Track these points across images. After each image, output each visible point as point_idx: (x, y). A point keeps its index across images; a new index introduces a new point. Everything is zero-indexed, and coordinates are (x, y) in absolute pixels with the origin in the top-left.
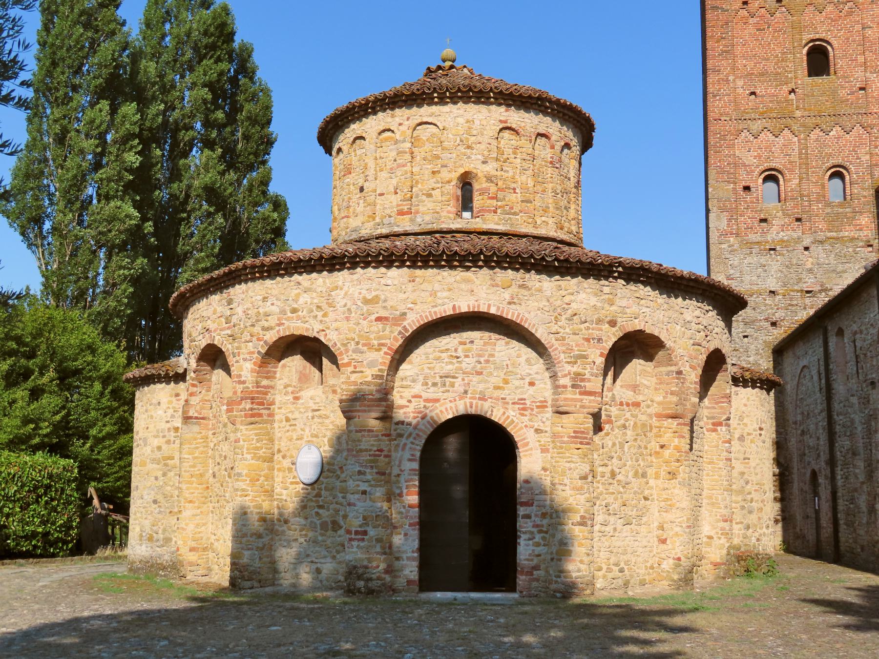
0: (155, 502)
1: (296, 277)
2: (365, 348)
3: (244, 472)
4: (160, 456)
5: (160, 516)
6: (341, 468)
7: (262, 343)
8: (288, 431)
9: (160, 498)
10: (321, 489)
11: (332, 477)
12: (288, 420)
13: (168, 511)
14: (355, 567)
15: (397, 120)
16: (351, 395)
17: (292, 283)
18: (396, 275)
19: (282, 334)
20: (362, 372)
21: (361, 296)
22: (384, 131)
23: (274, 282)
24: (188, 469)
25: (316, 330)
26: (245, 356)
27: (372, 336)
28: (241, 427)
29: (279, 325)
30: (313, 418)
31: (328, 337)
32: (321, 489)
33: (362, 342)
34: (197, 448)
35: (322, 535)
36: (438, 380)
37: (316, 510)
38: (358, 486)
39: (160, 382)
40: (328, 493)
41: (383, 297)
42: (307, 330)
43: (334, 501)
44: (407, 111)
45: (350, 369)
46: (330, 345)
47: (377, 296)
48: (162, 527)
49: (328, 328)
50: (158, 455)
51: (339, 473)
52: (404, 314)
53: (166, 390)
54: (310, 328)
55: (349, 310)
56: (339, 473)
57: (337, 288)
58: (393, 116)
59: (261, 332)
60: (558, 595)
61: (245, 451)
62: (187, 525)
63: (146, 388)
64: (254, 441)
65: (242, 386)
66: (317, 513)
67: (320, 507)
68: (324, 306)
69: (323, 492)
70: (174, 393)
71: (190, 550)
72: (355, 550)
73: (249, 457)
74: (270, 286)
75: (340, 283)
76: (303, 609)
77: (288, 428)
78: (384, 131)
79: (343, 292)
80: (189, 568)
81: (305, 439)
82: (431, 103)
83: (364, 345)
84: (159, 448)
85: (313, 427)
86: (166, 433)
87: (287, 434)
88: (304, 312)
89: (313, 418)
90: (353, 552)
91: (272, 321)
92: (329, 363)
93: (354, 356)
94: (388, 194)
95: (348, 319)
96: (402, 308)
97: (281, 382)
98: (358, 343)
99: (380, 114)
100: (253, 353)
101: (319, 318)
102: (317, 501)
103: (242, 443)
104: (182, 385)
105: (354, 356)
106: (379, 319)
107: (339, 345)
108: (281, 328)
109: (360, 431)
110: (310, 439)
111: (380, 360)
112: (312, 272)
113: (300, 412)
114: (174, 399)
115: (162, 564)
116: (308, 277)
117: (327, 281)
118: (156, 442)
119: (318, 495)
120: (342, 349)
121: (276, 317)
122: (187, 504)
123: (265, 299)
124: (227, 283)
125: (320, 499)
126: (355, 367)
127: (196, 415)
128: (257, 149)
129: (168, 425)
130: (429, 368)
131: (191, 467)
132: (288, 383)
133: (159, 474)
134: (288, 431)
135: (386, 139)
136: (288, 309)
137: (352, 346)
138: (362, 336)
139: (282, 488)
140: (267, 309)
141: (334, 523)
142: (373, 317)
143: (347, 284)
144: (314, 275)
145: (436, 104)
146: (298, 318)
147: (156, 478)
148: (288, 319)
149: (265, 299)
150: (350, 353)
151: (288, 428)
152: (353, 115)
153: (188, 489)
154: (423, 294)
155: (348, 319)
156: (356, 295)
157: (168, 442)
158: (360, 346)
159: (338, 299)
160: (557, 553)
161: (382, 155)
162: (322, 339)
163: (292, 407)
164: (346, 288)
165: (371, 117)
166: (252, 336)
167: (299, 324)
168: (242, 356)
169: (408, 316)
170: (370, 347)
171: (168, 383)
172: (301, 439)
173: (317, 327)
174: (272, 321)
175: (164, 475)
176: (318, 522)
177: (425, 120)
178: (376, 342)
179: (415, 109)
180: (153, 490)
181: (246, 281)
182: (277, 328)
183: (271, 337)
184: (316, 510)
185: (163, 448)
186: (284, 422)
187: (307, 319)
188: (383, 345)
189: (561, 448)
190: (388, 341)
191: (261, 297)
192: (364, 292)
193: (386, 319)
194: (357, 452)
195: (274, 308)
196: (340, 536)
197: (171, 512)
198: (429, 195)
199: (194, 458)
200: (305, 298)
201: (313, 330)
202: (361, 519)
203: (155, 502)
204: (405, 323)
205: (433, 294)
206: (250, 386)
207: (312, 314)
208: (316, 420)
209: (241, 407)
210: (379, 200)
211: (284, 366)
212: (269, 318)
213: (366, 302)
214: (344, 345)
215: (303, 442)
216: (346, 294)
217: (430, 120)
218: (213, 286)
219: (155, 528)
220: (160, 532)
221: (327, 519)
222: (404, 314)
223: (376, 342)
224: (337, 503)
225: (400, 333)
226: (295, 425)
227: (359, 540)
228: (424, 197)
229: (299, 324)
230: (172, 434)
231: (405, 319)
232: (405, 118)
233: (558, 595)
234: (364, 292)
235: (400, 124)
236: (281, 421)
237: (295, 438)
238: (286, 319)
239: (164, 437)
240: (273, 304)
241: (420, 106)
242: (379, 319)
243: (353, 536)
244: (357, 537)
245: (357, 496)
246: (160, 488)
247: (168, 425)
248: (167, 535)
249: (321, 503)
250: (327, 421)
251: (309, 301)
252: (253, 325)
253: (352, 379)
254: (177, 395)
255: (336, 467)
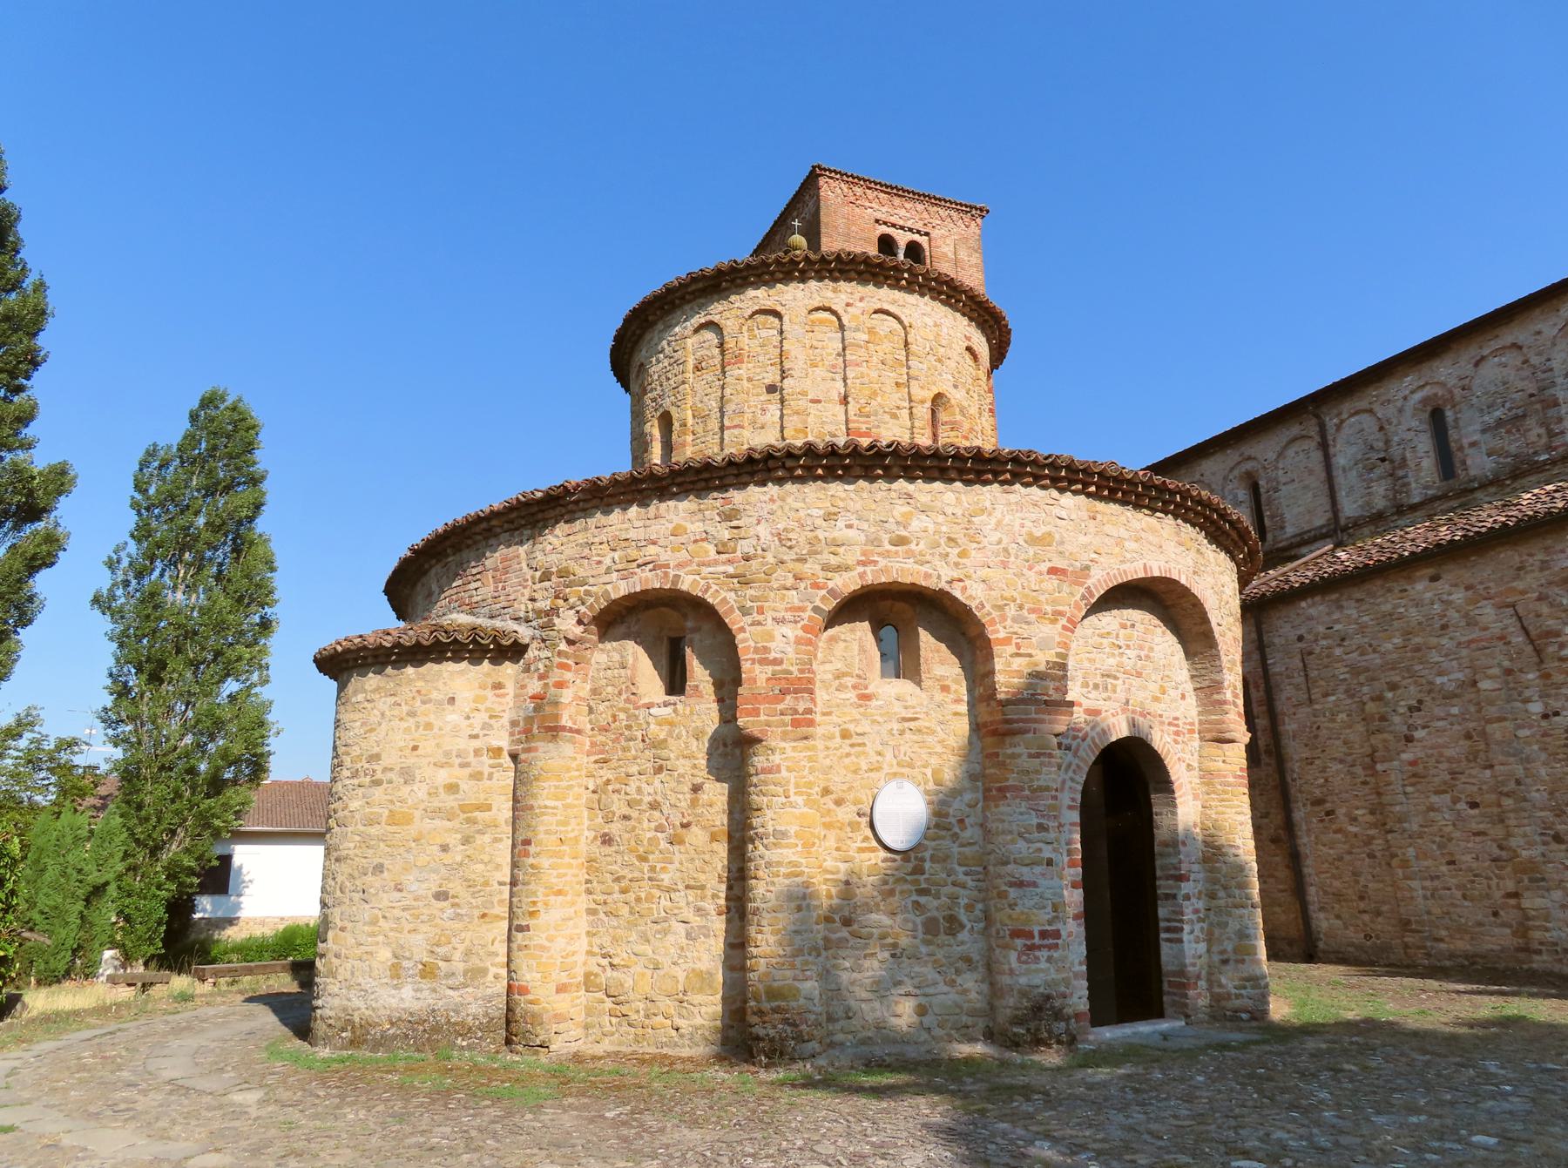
0: (441, 896)
1: (901, 484)
2: (1033, 617)
3: (793, 829)
4: (455, 804)
5: (457, 925)
6: (961, 821)
7: (824, 592)
8: (848, 755)
9: (455, 887)
10: (923, 860)
11: (943, 838)
12: (845, 735)
13: (477, 913)
14: (1048, 997)
15: (844, 297)
16: (1014, 694)
17: (893, 495)
18: (1071, 504)
19: (870, 579)
20: (1030, 656)
21: (1024, 531)
22: (817, 309)
23: (851, 487)
24: (554, 828)
25: (944, 578)
26: (779, 615)
27: (1042, 598)
28: (783, 744)
29: (863, 563)
30: (902, 733)
31: (969, 592)
32: (923, 860)
33: (1027, 606)
34: (572, 786)
35: (927, 943)
36: (1099, 680)
37: (915, 897)
38: (1040, 850)
39: (457, 658)
40: (937, 867)
41: (1057, 536)
42: (927, 576)
43: (950, 880)
44: (860, 288)
45: (1011, 649)
46: (973, 605)
47: (1049, 534)
48: (461, 948)
49: (969, 577)
50: (450, 801)
51: (957, 829)
52: (1087, 568)
53: (471, 674)
54: (933, 574)
55: (1006, 550)
56: (957, 829)
57: (983, 511)
58: (835, 291)
59: (821, 574)
60: (1244, 1016)
61: (792, 790)
62: (550, 939)
63: (410, 670)
64: (806, 772)
65: (769, 669)
66: (916, 903)
67: (922, 892)
68: (962, 540)
69: (927, 865)
70: (490, 681)
71: (558, 991)
72: (1043, 965)
73: (800, 800)
74: (843, 495)
75: (988, 504)
76: (1103, 1085)
77: (848, 749)
78: (817, 309)
79: (993, 521)
80: (555, 1028)
81: (886, 769)
82: (896, 286)
83: (1032, 611)
84: (452, 788)
85: (902, 749)
86: (471, 758)
87: (847, 761)
88: (922, 546)
89: (902, 733)
90: (1042, 970)
91: (851, 556)
92: (932, 640)
93: (1016, 628)
94: (830, 401)
95: (1005, 565)
96: (1085, 558)
97: (828, 667)
98: (1021, 607)
99: (813, 284)
100: (802, 609)
101: (953, 557)
102: (917, 882)
103: (784, 773)
104: (509, 669)
105: (1016, 628)
106: (1053, 571)
107: (988, 607)
108: (869, 569)
109: (1038, 755)
110: (895, 769)
111: (1058, 639)
112: (933, 480)
113: (874, 722)
114: (489, 693)
115: (462, 1024)
116: (927, 486)
117: (963, 497)
118: (443, 776)
119: (919, 870)
120: (995, 614)
121: (857, 549)
122: (552, 898)
123: (829, 517)
124: (727, 481)
125: (922, 878)
126: (1018, 646)
127: (569, 724)
128: (15, 367)
129: (476, 743)
130: (1089, 660)
131: (559, 823)
132: (845, 669)
133: (453, 839)
134: (848, 755)
135: (822, 322)
136: (885, 538)
137: (1011, 611)
138: (1026, 596)
139: (836, 860)
140: (836, 534)
141: (952, 919)
142: (1044, 567)
143: (999, 508)
144: (938, 485)
145: (901, 288)
146: (910, 554)
147: (445, 848)
148: (887, 555)
149: (829, 517)
150: (1009, 622)
151: (848, 749)
152: (759, 276)
153: (552, 867)
154: (1107, 540)
155: (1005, 565)
156: (1017, 527)
157: (477, 776)
158: (1025, 612)
159: (986, 530)
160: (1235, 951)
161: (815, 343)
162: (957, 594)
163: (855, 713)
164: (997, 514)
165: (794, 285)
166: (797, 578)
167: (910, 565)
168: (769, 615)
169: (1093, 572)
170: (1042, 615)
171: (476, 660)
172: (878, 769)
173: (947, 573)
174: (851, 556)
175: (466, 841)
176: (919, 920)
177: (886, 307)
178: (1049, 609)
179: (871, 287)
180: (435, 871)
181: (780, 481)
182: (861, 569)
183: (848, 583)
184: (915, 897)
185: (463, 786)
186: (838, 740)
187: (928, 558)
188: (1061, 614)
189: (1225, 792)
190: (1066, 608)
191: (821, 512)
192: (1028, 524)
193: (1063, 572)
194: (1033, 791)
195: (851, 533)
196: (962, 943)
197: (484, 916)
198: (894, 416)
199: (566, 807)
200: (918, 523)
201: (939, 577)
202: (1049, 909)
203: (441, 896)
204: (1089, 582)
205: (1120, 542)
206: (794, 669)
207: (937, 551)
208: (908, 735)
209: (781, 707)
210: (813, 408)
211: (833, 639)
212: (841, 550)
213: (1033, 540)
214: (1001, 608)
215: (881, 775)
216: (999, 523)
217: (892, 309)
218: (679, 485)
219: (441, 951)
220: (457, 956)
221: (936, 914)
222: (1087, 568)
223: (1049, 609)
224: (954, 884)
225: (1083, 597)
226: (864, 744)
227: (1050, 947)
228: (887, 417)
229: (910, 565)
230: (486, 760)
231: (1088, 577)
232: (857, 296)
233: (1244, 1016)
234: (1028, 524)
235: (848, 305)
236: (831, 737)
237: (864, 767)
238: (879, 554)
239: (463, 765)
240: (850, 526)
241: (878, 285)
242: (1053, 571)
243: (1037, 941)
244: (1046, 942)
245: (1038, 869)
246: (454, 868)
247: (476, 743)
248: (475, 961)
249: (924, 886)
250: (929, 739)
251: (931, 527)
252: (802, 560)
253: (1015, 667)
254: (498, 686)
255: (953, 820)
